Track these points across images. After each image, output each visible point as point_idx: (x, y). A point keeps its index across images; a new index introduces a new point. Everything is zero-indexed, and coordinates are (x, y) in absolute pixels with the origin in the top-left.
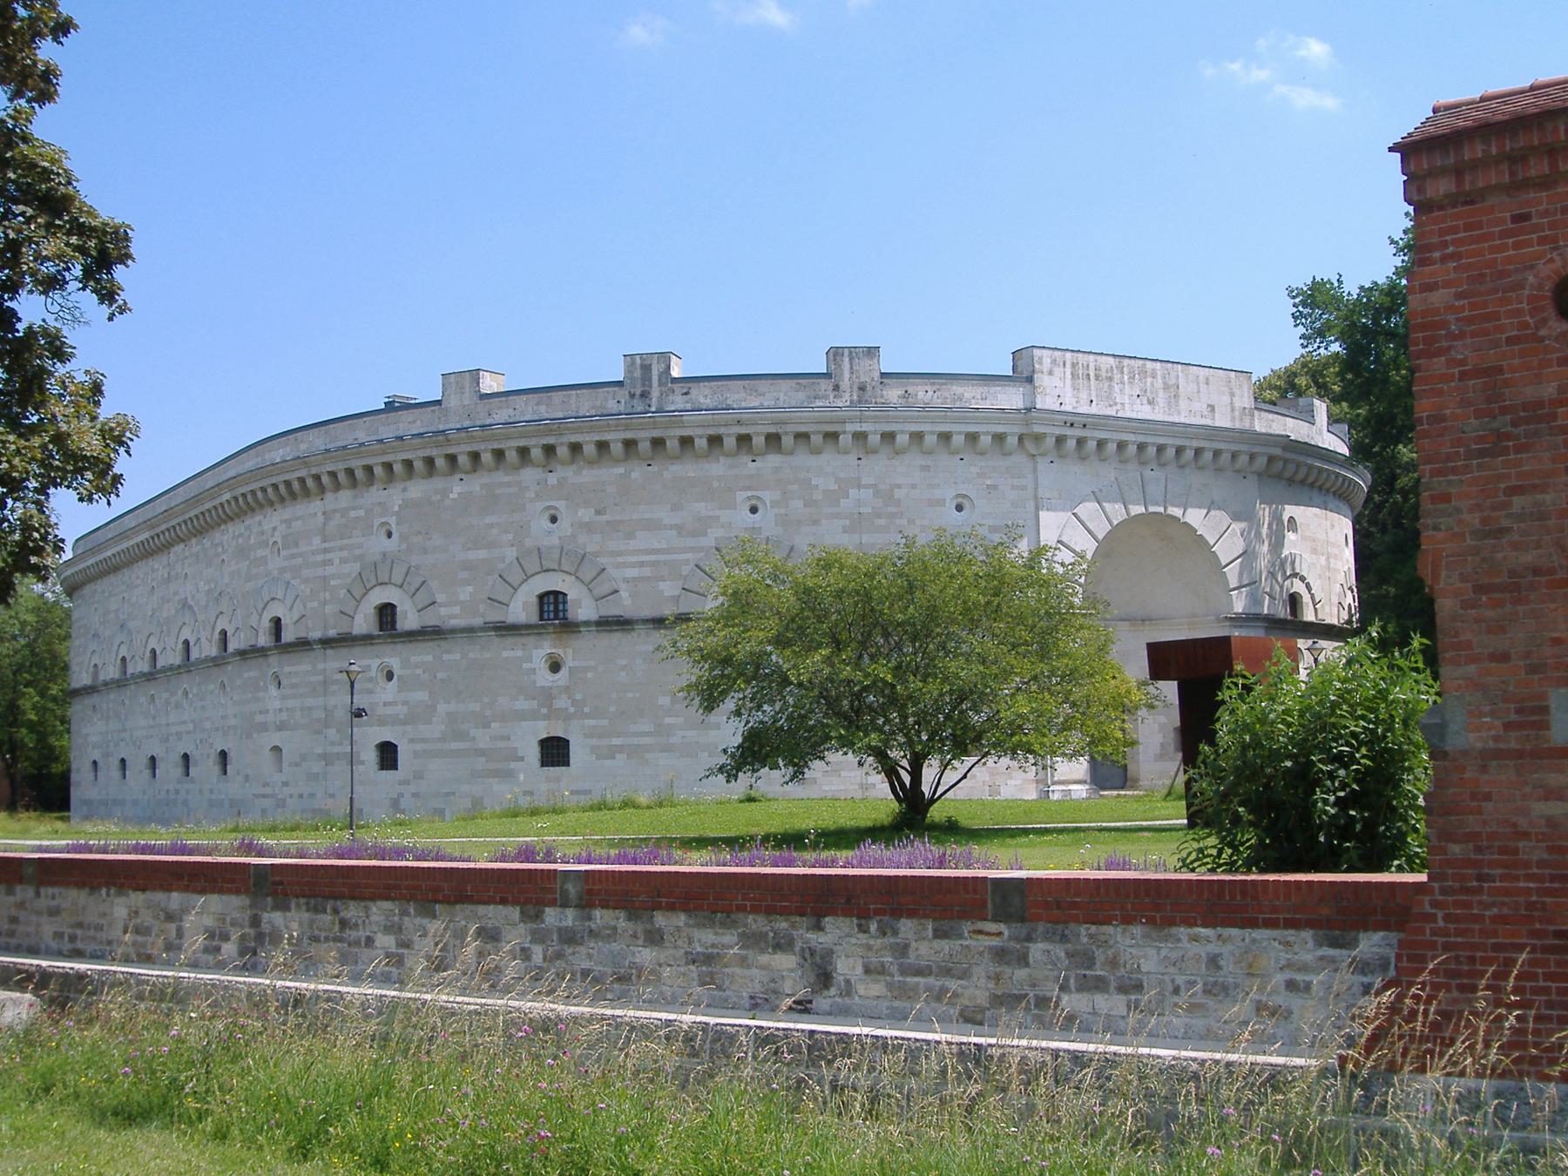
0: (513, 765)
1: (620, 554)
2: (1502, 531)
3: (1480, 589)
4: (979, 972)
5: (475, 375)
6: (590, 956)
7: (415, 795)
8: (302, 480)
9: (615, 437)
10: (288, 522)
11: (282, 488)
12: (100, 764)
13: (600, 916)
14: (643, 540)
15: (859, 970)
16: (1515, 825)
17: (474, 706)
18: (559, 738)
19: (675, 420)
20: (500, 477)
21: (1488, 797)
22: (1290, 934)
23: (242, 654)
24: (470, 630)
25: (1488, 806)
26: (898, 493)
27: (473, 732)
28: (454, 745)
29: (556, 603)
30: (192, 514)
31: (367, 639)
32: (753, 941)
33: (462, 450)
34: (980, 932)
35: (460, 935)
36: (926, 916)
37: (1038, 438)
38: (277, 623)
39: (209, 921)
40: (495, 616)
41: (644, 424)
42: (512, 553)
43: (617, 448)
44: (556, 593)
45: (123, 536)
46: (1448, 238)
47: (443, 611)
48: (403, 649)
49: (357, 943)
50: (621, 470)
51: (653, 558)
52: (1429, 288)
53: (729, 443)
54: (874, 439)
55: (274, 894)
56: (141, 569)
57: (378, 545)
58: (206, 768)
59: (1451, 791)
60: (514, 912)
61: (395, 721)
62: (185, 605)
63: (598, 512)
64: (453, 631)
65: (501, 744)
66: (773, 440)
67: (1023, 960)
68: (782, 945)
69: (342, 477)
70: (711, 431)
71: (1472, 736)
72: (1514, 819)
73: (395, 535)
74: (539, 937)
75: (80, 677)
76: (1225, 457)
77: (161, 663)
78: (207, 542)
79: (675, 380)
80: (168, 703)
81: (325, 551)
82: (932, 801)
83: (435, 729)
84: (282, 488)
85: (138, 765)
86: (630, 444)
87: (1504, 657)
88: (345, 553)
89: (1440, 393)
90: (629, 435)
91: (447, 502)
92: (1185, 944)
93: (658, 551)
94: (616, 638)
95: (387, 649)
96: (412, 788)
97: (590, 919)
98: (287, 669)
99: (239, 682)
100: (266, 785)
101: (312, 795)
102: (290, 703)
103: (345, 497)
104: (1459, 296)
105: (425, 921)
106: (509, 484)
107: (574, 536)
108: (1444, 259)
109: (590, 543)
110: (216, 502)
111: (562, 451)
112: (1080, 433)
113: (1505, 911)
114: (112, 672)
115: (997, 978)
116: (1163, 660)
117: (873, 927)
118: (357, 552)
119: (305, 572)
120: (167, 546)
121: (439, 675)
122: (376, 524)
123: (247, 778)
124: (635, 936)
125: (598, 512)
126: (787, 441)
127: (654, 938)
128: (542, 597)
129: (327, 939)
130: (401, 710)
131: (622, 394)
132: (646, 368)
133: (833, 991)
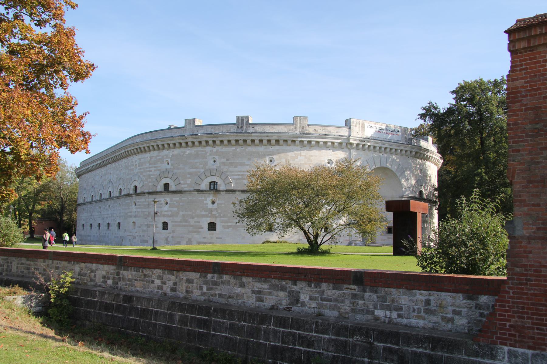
0: (200, 230)
1: (233, 172)
2: (539, 163)
3: (529, 182)
4: (347, 301)
5: (194, 120)
6: (221, 289)
7: (172, 237)
8: (144, 148)
9: (233, 139)
10: (140, 159)
11: (139, 149)
12: (85, 225)
13: (226, 277)
14: (240, 168)
15: (308, 298)
16: (540, 263)
17: (190, 213)
18: (213, 223)
19: (250, 135)
20: (200, 149)
21: (530, 252)
22: (454, 294)
23: (126, 196)
24: (190, 191)
25: (531, 255)
26: (312, 158)
27: (189, 220)
28: (184, 224)
29: (214, 185)
30: (113, 156)
31: (161, 192)
32: (275, 287)
33: (189, 141)
34: (348, 288)
35: (181, 280)
36: (330, 283)
37: (352, 144)
38: (136, 187)
39: (104, 273)
40: (197, 188)
41: (241, 135)
42: (202, 170)
43: (233, 142)
44: (214, 182)
45: (94, 161)
46: (523, 63)
47: (182, 186)
48: (170, 195)
49: (149, 282)
50: (234, 148)
51: (242, 173)
52: (516, 80)
53: (265, 142)
54: (306, 143)
55: (124, 266)
56: (98, 171)
57: (164, 166)
58: (114, 227)
59: (517, 250)
60: (198, 275)
61: (167, 216)
62: (110, 181)
63: (227, 160)
64: (185, 191)
65: (197, 224)
66: (277, 141)
67: (363, 298)
68: (283, 289)
69: (156, 147)
70: (260, 138)
71: (525, 232)
72: (540, 260)
73: (170, 164)
74: (206, 283)
75: (80, 201)
76: (404, 152)
77: (103, 197)
78: (117, 164)
79: (250, 124)
80: (104, 208)
81: (150, 168)
82: (321, 244)
83: (178, 219)
84: (139, 149)
85: (95, 225)
86: (237, 141)
87: (539, 205)
88: (155, 169)
89: (517, 115)
90: (237, 139)
91: (185, 155)
92: (418, 296)
93: (243, 171)
94: (231, 195)
95: (166, 195)
96: (172, 235)
97: (222, 278)
98: (138, 200)
99: (124, 203)
100: (130, 232)
101: (143, 236)
102: (138, 210)
103: (156, 153)
104: (526, 82)
105: (170, 276)
106: (202, 151)
107: (220, 166)
108: (521, 70)
109: (225, 168)
110: (120, 153)
111: (218, 142)
112: (364, 143)
113: (536, 292)
114: (89, 199)
115: (353, 303)
116: (390, 206)
117: (313, 285)
118: (159, 168)
119: (144, 174)
120: (106, 165)
121: (181, 204)
122: (165, 160)
123: (125, 230)
124: (236, 284)
125: (227, 160)
126: (281, 142)
127: (242, 285)
128: (210, 183)
129: (140, 280)
130: (170, 213)
131: (235, 127)
132: (242, 120)
133: (299, 305)
